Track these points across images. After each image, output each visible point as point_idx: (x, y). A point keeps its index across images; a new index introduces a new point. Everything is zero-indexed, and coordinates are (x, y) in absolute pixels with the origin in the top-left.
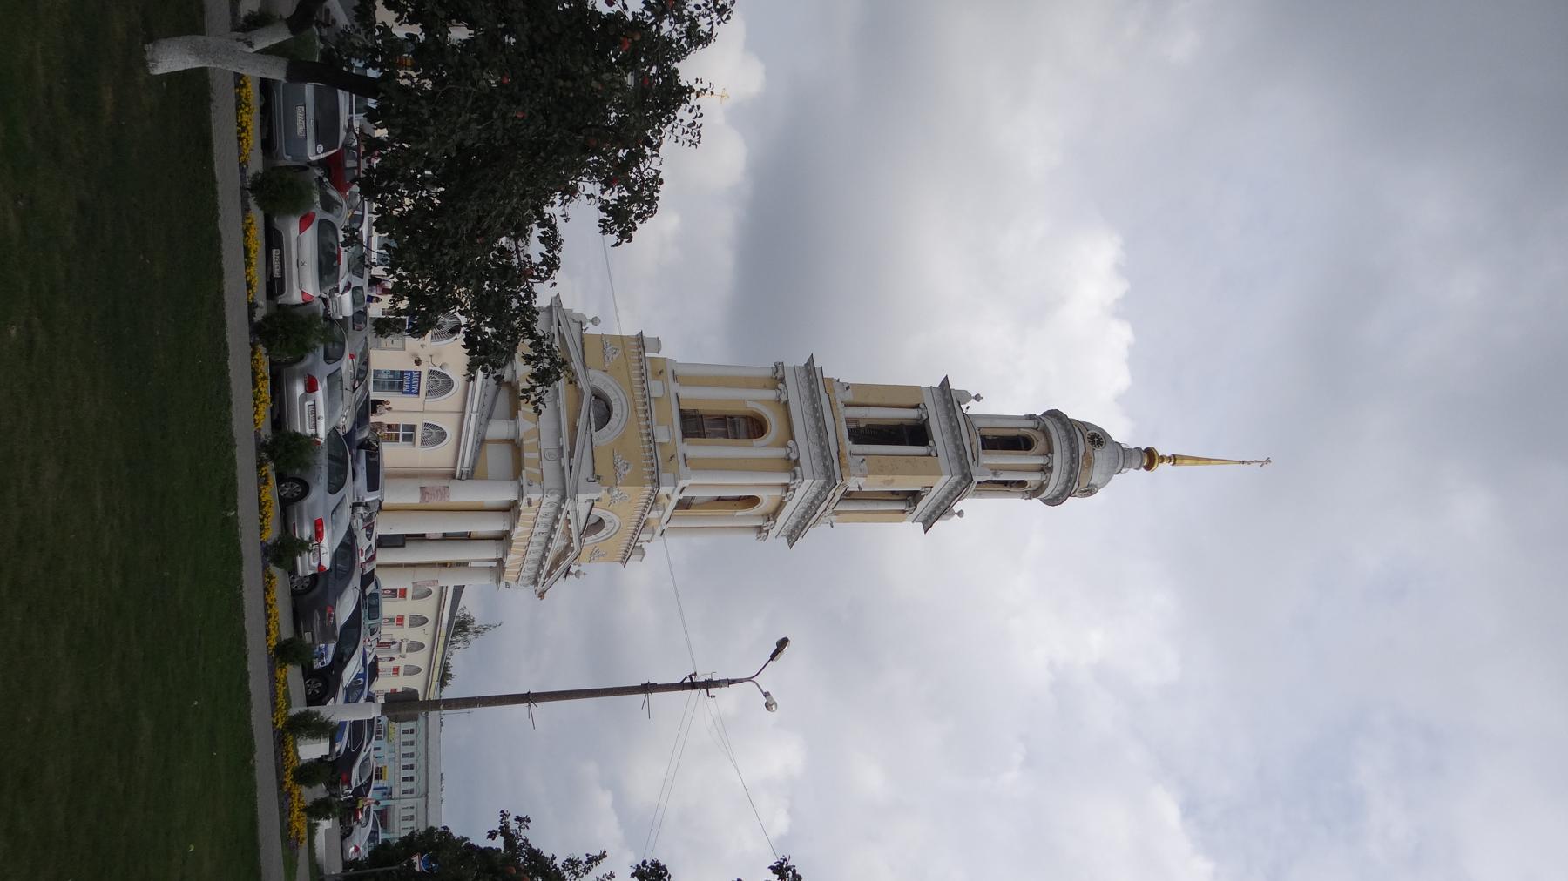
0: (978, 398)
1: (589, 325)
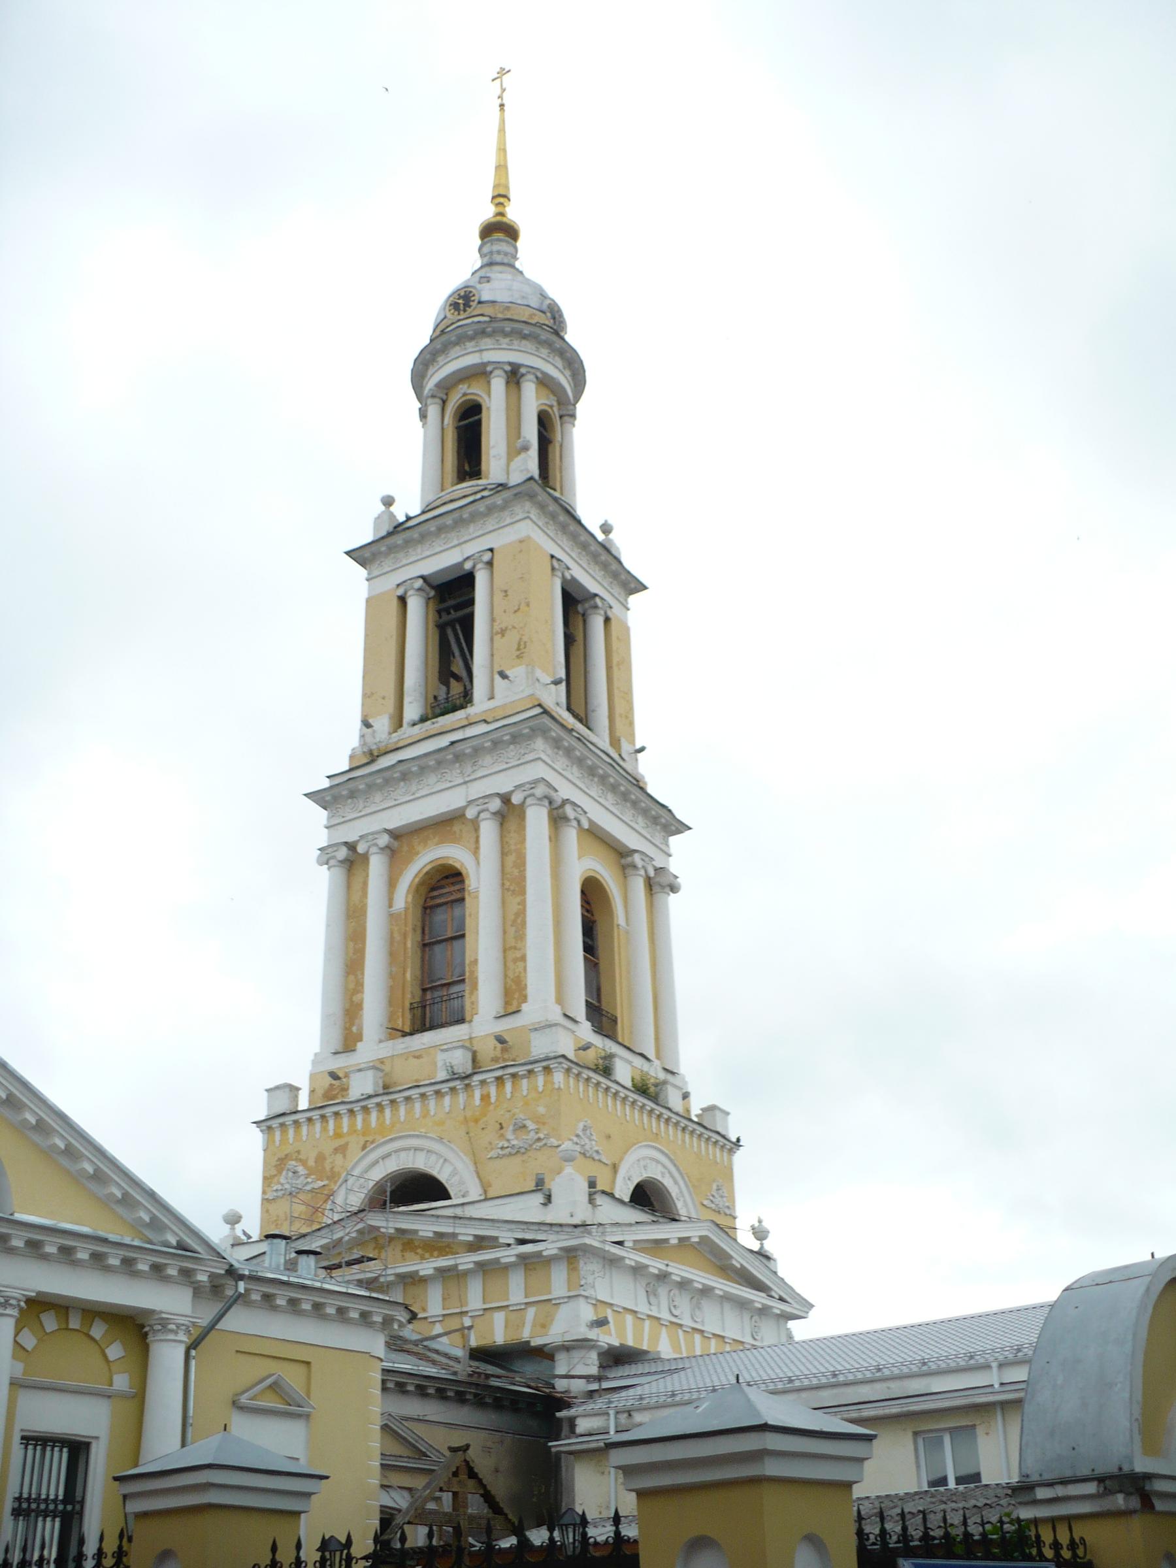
0: (388, 502)
1: (239, 1229)
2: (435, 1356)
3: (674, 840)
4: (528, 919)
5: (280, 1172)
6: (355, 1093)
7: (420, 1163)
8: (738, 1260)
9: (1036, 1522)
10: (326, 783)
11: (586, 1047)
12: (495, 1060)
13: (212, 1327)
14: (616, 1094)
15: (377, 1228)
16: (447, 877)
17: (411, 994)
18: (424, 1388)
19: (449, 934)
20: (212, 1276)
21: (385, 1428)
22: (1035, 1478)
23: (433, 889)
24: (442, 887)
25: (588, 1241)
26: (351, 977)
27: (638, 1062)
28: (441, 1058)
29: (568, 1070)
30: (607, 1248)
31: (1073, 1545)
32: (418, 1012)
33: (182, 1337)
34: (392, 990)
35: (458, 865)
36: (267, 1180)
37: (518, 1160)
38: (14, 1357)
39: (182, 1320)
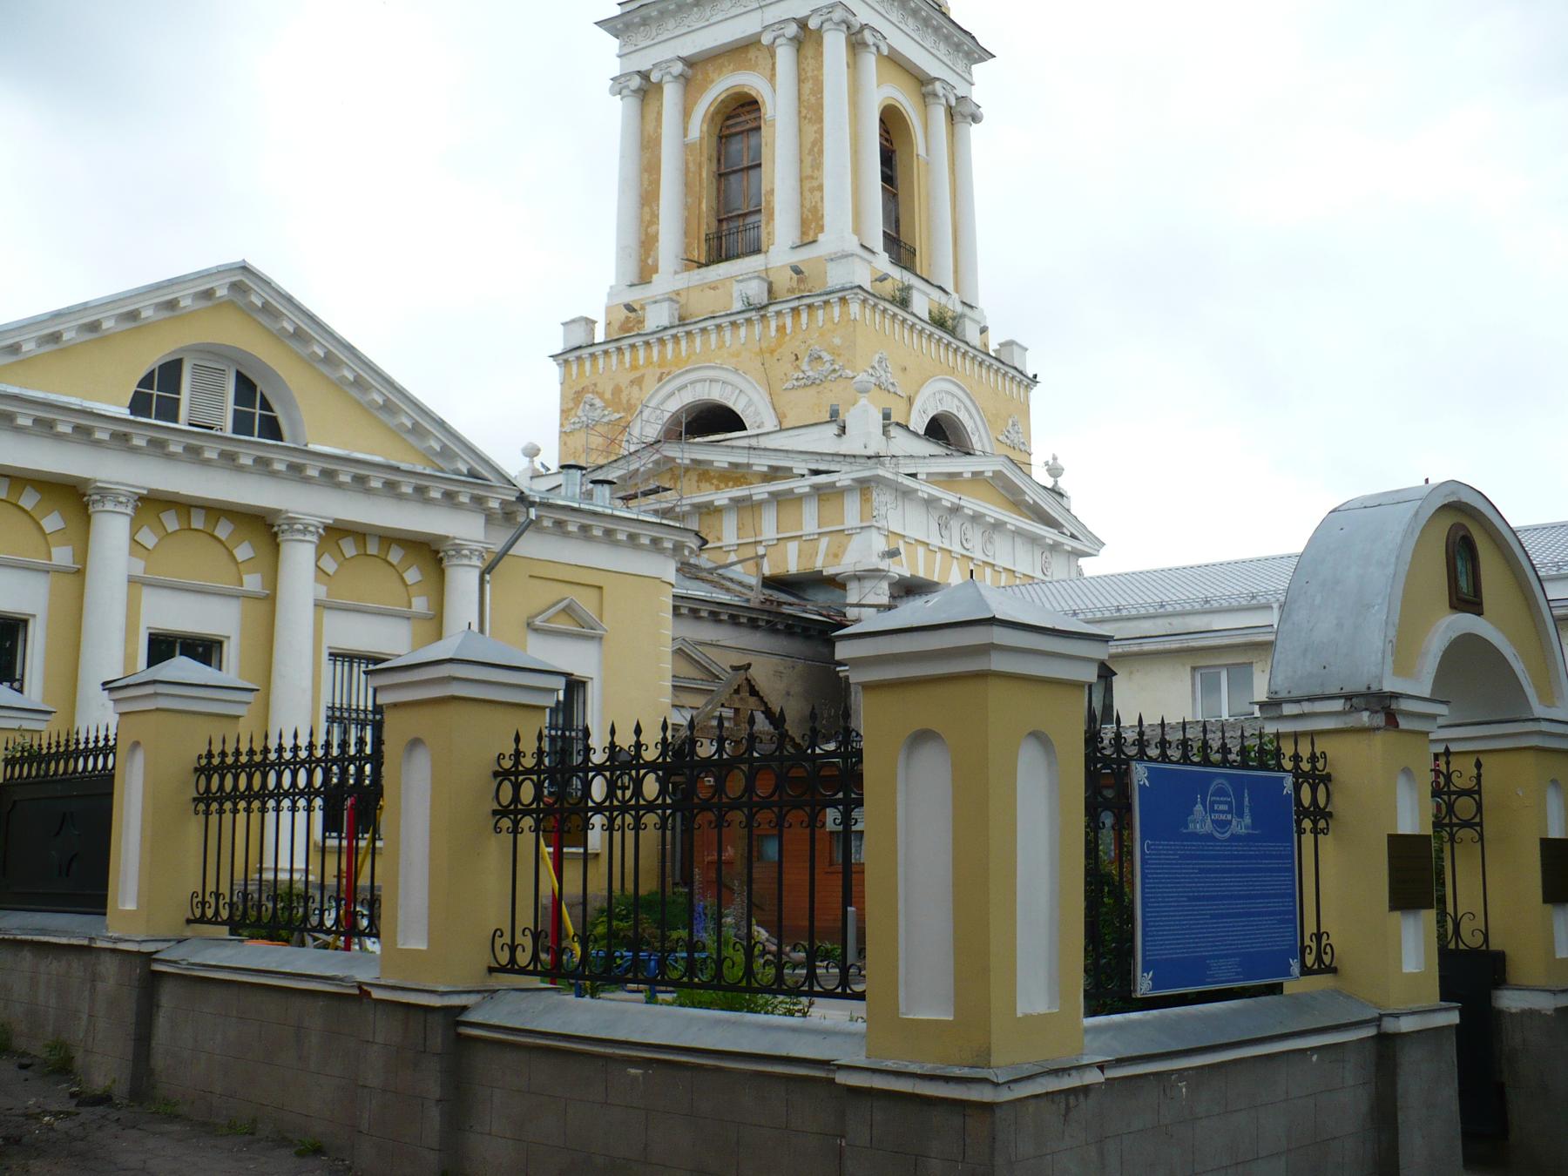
1: (538, 460)
2: (729, 584)
3: (977, 69)
4: (826, 147)
5: (577, 405)
6: (651, 324)
7: (716, 394)
8: (1031, 496)
9: (1278, 736)
10: (617, 11)
11: (883, 279)
12: (791, 291)
13: (504, 553)
14: (913, 326)
15: (673, 459)
16: (742, 106)
17: (707, 225)
18: (716, 614)
19: (745, 164)
20: (504, 503)
21: (679, 652)
22: (1283, 694)
23: (728, 118)
24: (739, 115)
25: (881, 472)
26: (647, 209)
27: (936, 294)
28: (736, 289)
29: (864, 301)
30: (900, 480)
31: (1313, 758)
32: (715, 243)
33: (476, 562)
34: (687, 221)
35: (754, 94)
36: (565, 413)
37: (812, 391)
38: (317, 580)
39: (474, 546)
